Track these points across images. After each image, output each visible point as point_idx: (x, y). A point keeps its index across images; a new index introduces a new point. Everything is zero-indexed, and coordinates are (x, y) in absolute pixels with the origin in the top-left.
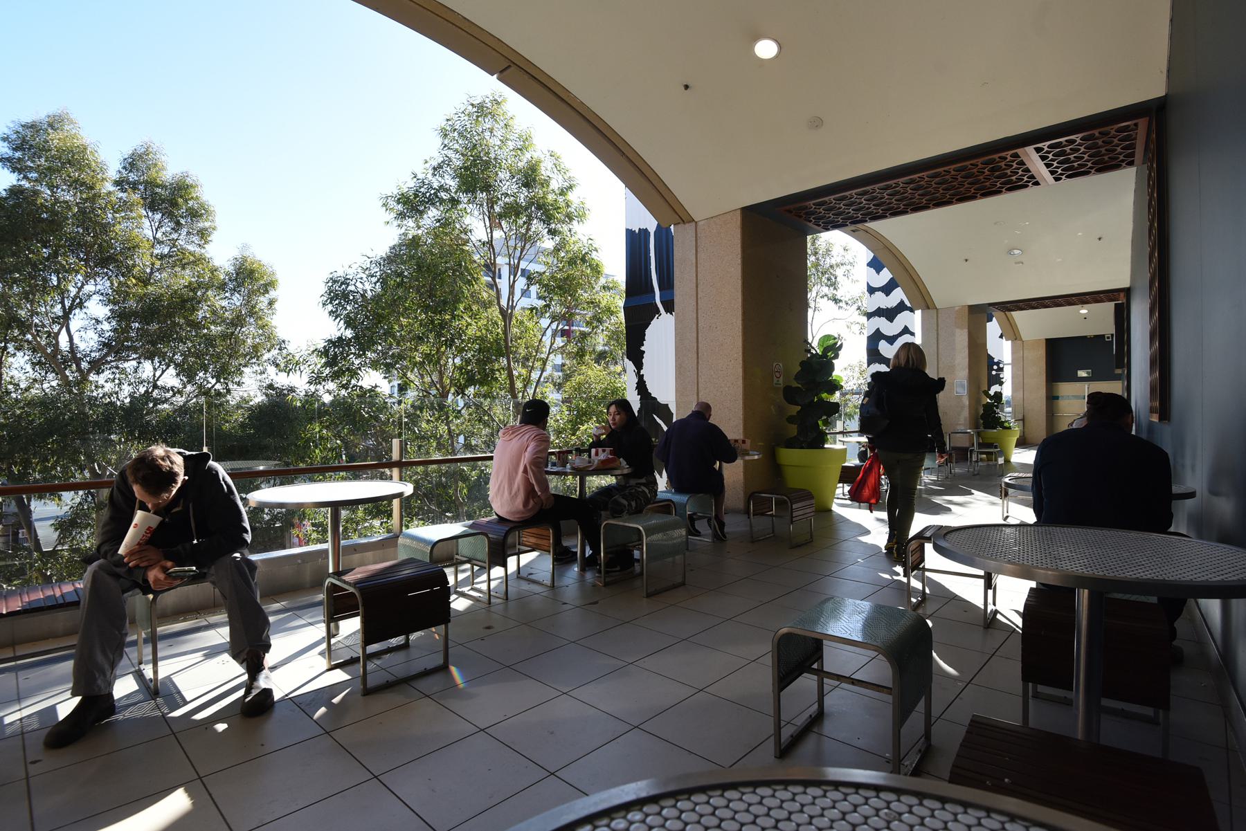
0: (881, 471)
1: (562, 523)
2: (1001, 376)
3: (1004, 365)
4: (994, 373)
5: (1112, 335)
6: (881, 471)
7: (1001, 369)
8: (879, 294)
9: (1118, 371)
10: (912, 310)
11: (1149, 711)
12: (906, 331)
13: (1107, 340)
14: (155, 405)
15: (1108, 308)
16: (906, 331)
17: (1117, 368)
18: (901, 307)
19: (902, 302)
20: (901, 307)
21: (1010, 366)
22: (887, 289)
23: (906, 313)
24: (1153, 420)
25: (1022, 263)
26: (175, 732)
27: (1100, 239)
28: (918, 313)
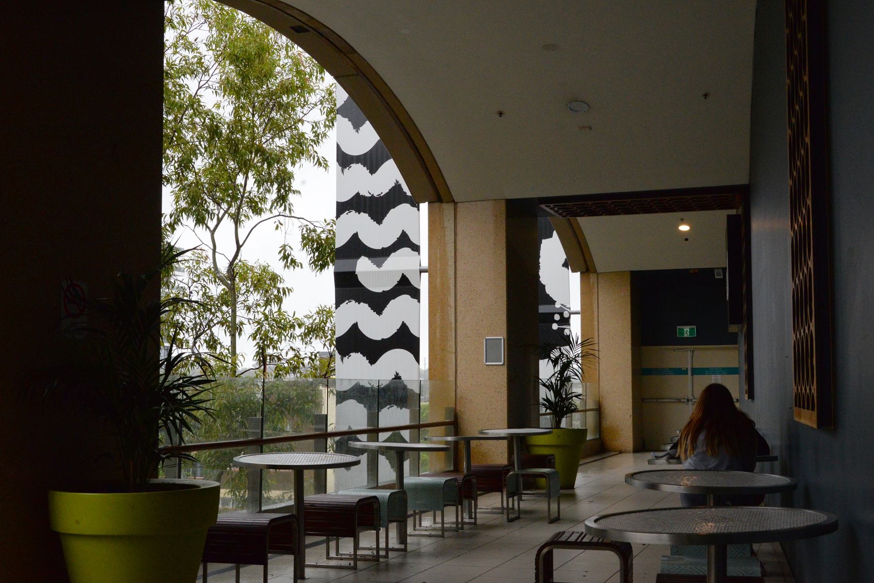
0: (162, 378)
1: (541, 412)
2: (567, 332)
3: (570, 314)
4: (555, 327)
5: (724, 269)
6: (162, 378)
7: (565, 321)
8: (358, 169)
9: (733, 328)
10: (415, 204)
11: (307, 521)
12: (404, 241)
13: (716, 277)
14: (244, 498)
15: (718, 219)
16: (404, 241)
17: (733, 322)
18: (394, 197)
19: (397, 187)
20: (394, 197)
21: (579, 316)
22: (372, 162)
23: (404, 208)
24: (803, 421)
25: (590, 128)
26: (422, 430)
27: (706, 95)
28: (424, 207)
